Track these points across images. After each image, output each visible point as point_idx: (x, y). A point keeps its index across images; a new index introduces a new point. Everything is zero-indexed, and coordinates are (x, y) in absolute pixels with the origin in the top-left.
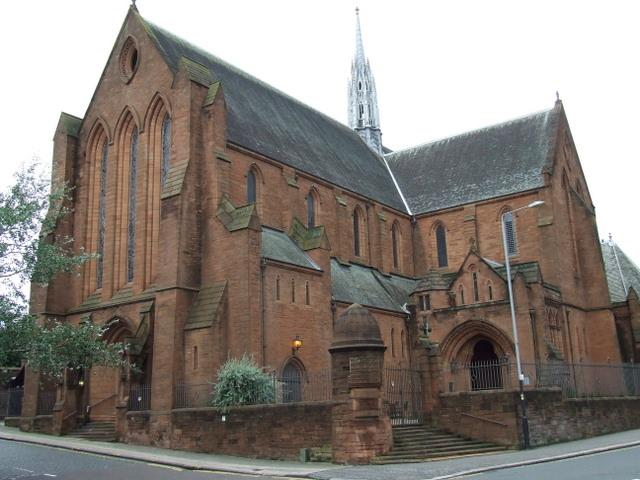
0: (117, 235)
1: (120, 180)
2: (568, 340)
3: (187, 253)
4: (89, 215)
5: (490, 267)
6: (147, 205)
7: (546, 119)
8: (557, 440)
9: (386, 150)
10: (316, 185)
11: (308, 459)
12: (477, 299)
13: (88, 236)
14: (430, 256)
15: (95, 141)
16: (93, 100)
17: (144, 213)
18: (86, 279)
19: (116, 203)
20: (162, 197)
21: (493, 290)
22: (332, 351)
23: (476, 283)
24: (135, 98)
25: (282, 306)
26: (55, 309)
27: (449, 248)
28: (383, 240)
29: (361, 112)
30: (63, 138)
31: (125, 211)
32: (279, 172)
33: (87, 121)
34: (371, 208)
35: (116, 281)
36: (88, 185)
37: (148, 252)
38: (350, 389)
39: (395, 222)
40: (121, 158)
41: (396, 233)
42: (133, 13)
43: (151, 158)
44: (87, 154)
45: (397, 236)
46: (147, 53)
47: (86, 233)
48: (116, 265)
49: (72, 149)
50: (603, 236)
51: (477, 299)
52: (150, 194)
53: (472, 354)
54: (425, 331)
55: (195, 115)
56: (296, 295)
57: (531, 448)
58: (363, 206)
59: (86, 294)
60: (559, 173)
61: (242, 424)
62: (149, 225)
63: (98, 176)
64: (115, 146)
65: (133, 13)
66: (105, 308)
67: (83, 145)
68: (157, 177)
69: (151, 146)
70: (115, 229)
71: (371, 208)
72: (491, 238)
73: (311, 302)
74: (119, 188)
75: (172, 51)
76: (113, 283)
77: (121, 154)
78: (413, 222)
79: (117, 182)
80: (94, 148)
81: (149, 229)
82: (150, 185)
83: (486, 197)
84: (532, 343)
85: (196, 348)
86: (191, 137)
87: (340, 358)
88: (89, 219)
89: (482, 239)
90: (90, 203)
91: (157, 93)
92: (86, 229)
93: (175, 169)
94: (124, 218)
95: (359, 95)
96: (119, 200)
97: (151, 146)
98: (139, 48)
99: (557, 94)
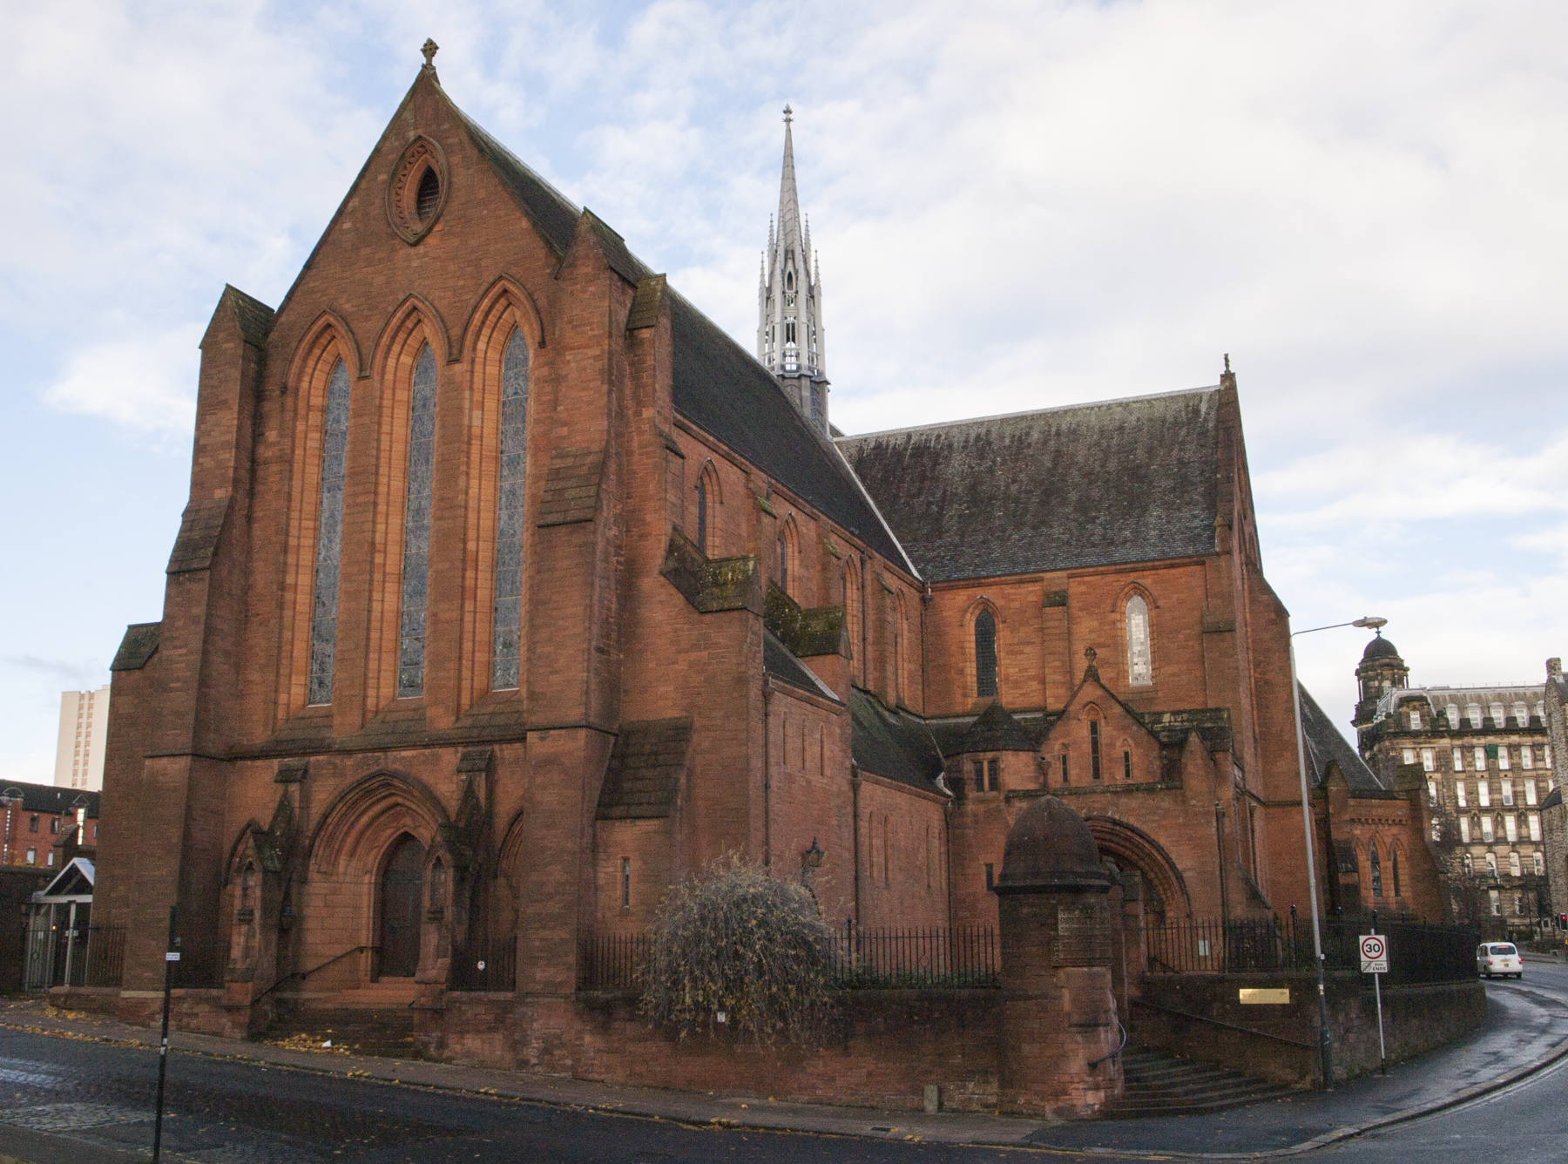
9: (835, 432)
13: (290, 580)
14: (961, 672)
15: (311, 363)
16: (308, 266)
18: (283, 680)
21: (1134, 759)
23: (1095, 743)
26: (213, 744)
31: (394, 536)
33: (283, 319)
35: (371, 692)
36: (291, 462)
37: (468, 636)
42: (426, 83)
46: (463, 178)
48: (373, 656)
49: (252, 374)
62: (470, 574)
65: (426, 83)
68: (489, 467)
73: (828, 772)
76: (365, 697)
85: (626, 859)
88: (293, 542)
90: (295, 504)
91: (501, 278)
94: (393, 549)
98: (430, 165)
99: (1227, 360)
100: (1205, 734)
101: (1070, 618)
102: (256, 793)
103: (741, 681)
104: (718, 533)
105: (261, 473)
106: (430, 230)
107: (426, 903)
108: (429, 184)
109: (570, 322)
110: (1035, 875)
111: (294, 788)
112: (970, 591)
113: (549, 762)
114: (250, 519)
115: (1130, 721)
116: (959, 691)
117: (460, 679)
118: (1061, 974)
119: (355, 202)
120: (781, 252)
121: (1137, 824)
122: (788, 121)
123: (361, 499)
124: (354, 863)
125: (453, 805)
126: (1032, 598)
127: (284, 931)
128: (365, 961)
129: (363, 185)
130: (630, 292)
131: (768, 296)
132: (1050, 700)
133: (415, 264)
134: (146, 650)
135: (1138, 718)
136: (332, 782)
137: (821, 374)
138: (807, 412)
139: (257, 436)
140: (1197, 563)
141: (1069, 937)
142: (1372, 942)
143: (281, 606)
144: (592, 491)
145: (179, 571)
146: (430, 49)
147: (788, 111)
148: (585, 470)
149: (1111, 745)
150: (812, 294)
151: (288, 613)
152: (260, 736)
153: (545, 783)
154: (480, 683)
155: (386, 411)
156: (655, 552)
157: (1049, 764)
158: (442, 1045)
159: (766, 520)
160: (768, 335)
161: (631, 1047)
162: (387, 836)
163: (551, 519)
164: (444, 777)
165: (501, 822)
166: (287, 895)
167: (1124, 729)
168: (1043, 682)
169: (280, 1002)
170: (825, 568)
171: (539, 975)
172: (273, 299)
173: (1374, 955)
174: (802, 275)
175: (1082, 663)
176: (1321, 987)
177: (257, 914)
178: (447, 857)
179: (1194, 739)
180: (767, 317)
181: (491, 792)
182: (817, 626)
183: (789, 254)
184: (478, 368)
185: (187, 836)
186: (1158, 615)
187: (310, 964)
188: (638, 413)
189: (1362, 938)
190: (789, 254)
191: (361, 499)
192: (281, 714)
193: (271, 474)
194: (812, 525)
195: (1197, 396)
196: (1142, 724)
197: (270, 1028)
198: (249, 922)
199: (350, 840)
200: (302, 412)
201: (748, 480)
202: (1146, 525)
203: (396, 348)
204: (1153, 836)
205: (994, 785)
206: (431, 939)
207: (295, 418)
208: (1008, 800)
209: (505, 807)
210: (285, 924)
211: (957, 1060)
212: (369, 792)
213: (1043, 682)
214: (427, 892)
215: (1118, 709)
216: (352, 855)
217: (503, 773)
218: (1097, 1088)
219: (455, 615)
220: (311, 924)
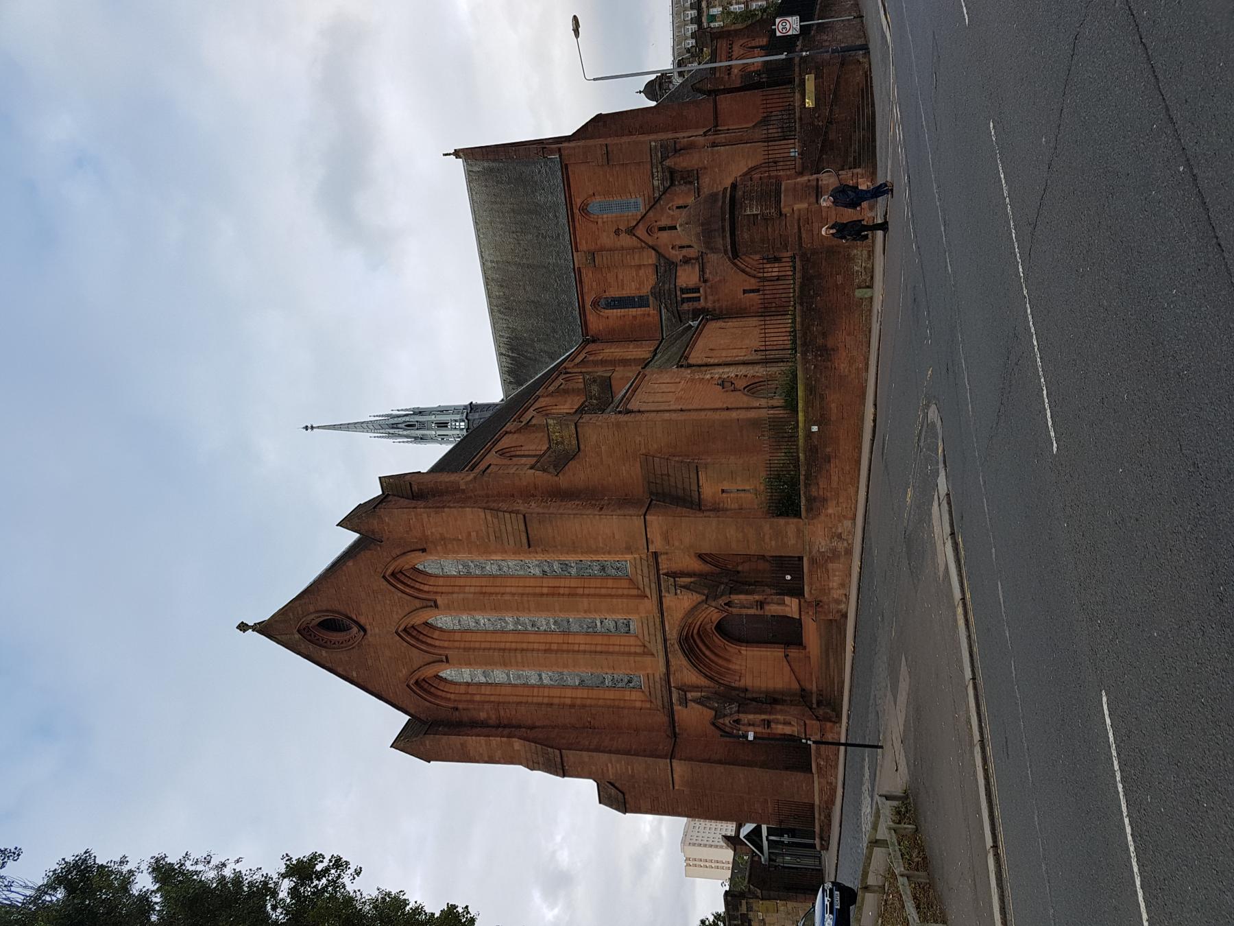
0: (571, 647)
1: (497, 646)
6: (535, 595)
13: (568, 701)
14: (635, 317)
15: (440, 693)
17: (544, 599)
19: (527, 650)
21: (681, 203)
27: (626, 293)
33: (412, 711)
35: (633, 649)
36: (499, 703)
37: (597, 591)
42: (264, 629)
43: (472, 589)
44: (455, 705)
52: (520, 590)
61: (822, 397)
62: (562, 591)
64: (449, 653)
65: (264, 629)
70: (563, 651)
76: (636, 653)
78: (590, 339)
79: (500, 649)
80: (448, 696)
82: (508, 590)
88: (546, 700)
90: (524, 700)
91: (384, 577)
96: (525, 646)
97: (456, 589)
98: (316, 627)
100: (664, 158)
101: (601, 250)
102: (693, 716)
103: (618, 425)
105: (506, 722)
106: (357, 623)
107: (752, 612)
108: (331, 625)
109: (407, 532)
111: (689, 695)
113: (666, 538)
114: (532, 728)
115: (658, 206)
116: (647, 319)
117: (622, 596)
118: (784, 211)
119: (340, 670)
120: (392, 431)
122: (312, 428)
123: (519, 660)
124: (734, 660)
125: (698, 598)
127: (775, 701)
128: (794, 652)
129: (329, 665)
130: (390, 498)
131: (422, 439)
132: (650, 262)
133: (377, 630)
134: (613, 791)
135: (657, 201)
136: (685, 671)
137: (465, 407)
138: (488, 414)
140: (567, 169)
143: (584, 706)
144: (507, 515)
145: (563, 771)
146: (243, 627)
147: (306, 428)
148: (495, 521)
150: (420, 412)
151: (588, 702)
152: (662, 718)
153: (684, 539)
154: (625, 584)
155: (467, 645)
156: (542, 478)
158: (838, 602)
159: (534, 422)
160: (443, 439)
161: (834, 485)
162: (718, 640)
163: (524, 540)
164: (680, 604)
165: (706, 568)
166: (754, 699)
168: (639, 267)
169: (819, 703)
171: (792, 542)
172: (401, 719)
174: (407, 419)
175: (626, 240)
177: (764, 717)
178: (725, 599)
179: (667, 163)
180: (432, 439)
181: (689, 575)
182: (595, 389)
183: (394, 426)
184: (439, 589)
185: (720, 762)
187: (795, 686)
189: (778, 34)
190: (394, 426)
191: (519, 660)
192: (648, 705)
194: (541, 399)
196: (660, 198)
197: (833, 710)
198: (769, 722)
199: (720, 662)
200: (469, 697)
202: (545, 204)
203: (429, 641)
205: (697, 290)
206: (773, 609)
207: (472, 701)
209: (696, 565)
210: (772, 700)
211: (840, 279)
212: (691, 650)
213: (639, 267)
214: (744, 611)
215: (651, 214)
216: (729, 661)
217: (675, 567)
219: (585, 600)
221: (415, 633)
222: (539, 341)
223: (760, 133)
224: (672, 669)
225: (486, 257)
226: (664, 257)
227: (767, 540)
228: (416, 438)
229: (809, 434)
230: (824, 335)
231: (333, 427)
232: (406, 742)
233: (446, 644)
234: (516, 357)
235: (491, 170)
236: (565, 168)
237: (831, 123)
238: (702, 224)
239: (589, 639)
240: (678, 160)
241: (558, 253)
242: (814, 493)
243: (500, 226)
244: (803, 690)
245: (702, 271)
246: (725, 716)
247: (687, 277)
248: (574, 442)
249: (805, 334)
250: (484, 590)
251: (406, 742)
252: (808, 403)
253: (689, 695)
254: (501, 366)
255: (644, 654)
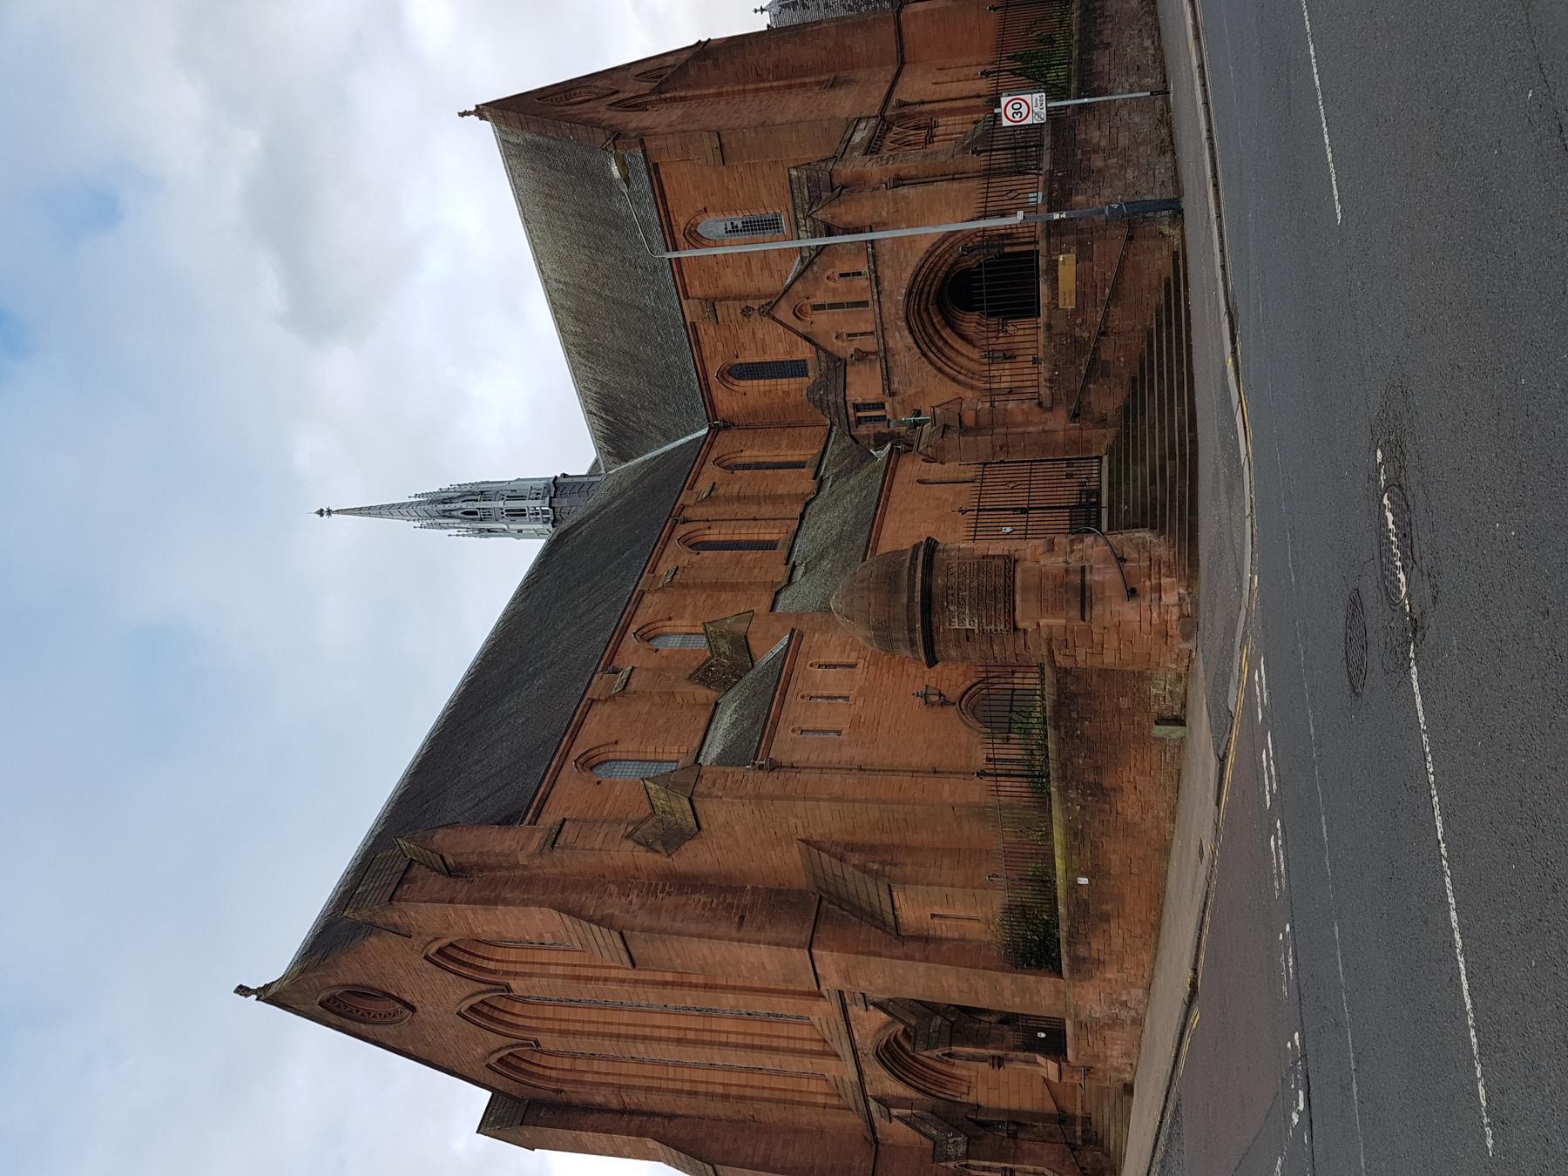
2: (959, 104)
3: (742, 918)
4: (679, 1085)
5: (799, 275)
7: (513, 139)
8: (1164, 131)
10: (633, 628)
11: (1180, 721)
12: (865, 304)
13: (719, 1090)
14: (786, 393)
15: (535, 1069)
18: (805, 1098)
20: (629, 965)
21: (846, 269)
22: (932, 661)
23: (833, 306)
24: (441, 997)
25: (856, 723)
28: (749, 492)
29: (521, 513)
30: (527, 1132)
32: (596, 708)
34: (687, 513)
35: (807, 1046)
38: (1016, 629)
39: (718, 462)
40: (564, 1026)
41: (739, 461)
42: (268, 994)
43: (560, 970)
44: (559, 1086)
45: (748, 460)
47: (713, 1095)
50: (761, 23)
51: (865, 304)
53: (975, 316)
54: (916, 424)
55: (462, 896)
56: (836, 693)
57: (1179, 191)
58: (682, 530)
59: (835, 1101)
60: (619, 117)
61: (1095, 846)
63: (603, 1066)
64: (540, 1037)
65: (270, 995)
66: (860, 1073)
67: (542, 1094)
69: (537, 969)
70: (704, 1043)
71: (687, 513)
72: (749, 271)
73: (852, 660)
74: (623, 1030)
75: (335, 934)
77: (556, 1025)
78: (721, 426)
80: (548, 1073)
81: (674, 1034)
83: (670, 276)
84: (956, 185)
86: (506, 902)
87: (944, 648)
88: (687, 1086)
89: (752, 287)
90: (656, 1084)
92: (706, 1094)
93: (574, 937)
94: (683, 1022)
95: (486, 516)
96: (647, 1032)
97: (537, 969)
99: (462, 115)
104: (642, 748)
110: (912, 643)
112: (713, 387)
115: (808, 274)
118: (1021, 625)
121: (910, 271)
122: (329, 512)
126: (711, 331)
137: (547, 487)
139: (603, 1109)
140: (657, 172)
141: (980, 617)
142: (1010, 111)
146: (243, 991)
147: (321, 513)
149: (835, 291)
151: (748, 1092)
156: (645, 858)
157: (857, 350)
158: (1119, 1070)
167: (817, 279)
170: (685, 586)
172: (481, 1098)
173: (1027, 108)
176: (1057, 216)
184: (511, 968)
186: (714, 209)
188: (525, 867)
189: (1006, 123)
193: (633, 1099)
194: (647, 599)
195: (505, 144)
200: (576, 1076)
201: (599, 700)
204: (921, 254)
205: (881, 406)
207: (583, 1083)
208: (892, 394)
211: (1125, 703)
215: (798, 286)
218: (1159, 589)
220: (1014, 1105)
221: (486, 1009)
222: (643, 407)
223: (976, 162)
224: (867, 1079)
225: (548, 271)
226: (826, 351)
227: (1007, 993)
228: (481, 530)
229: (1073, 887)
230: (1098, 769)
231: (359, 511)
232: (494, 1124)
233: (533, 1023)
234: (614, 424)
235: (538, 147)
236: (654, 169)
237: (1104, 334)
238: (874, 629)
239: (741, 1026)
240: (837, 210)
241: (657, 293)
242: (1082, 951)
243: (563, 233)
244: (1061, 1111)
245: (887, 377)
246: (948, 1158)
247: (863, 385)
248: (691, 820)
249: (1064, 766)
250: (578, 971)
251: (494, 1124)
252: (1070, 850)
253: (894, 1112)
254: (593, 429)
255: (823, 1054)
